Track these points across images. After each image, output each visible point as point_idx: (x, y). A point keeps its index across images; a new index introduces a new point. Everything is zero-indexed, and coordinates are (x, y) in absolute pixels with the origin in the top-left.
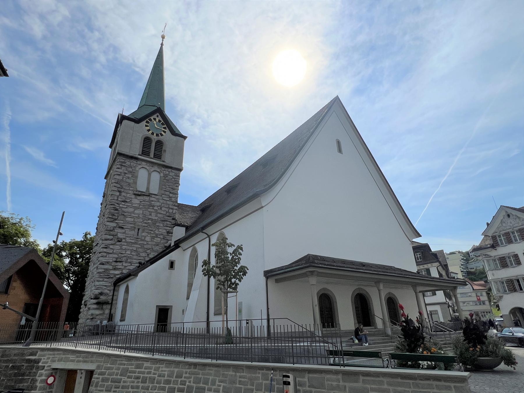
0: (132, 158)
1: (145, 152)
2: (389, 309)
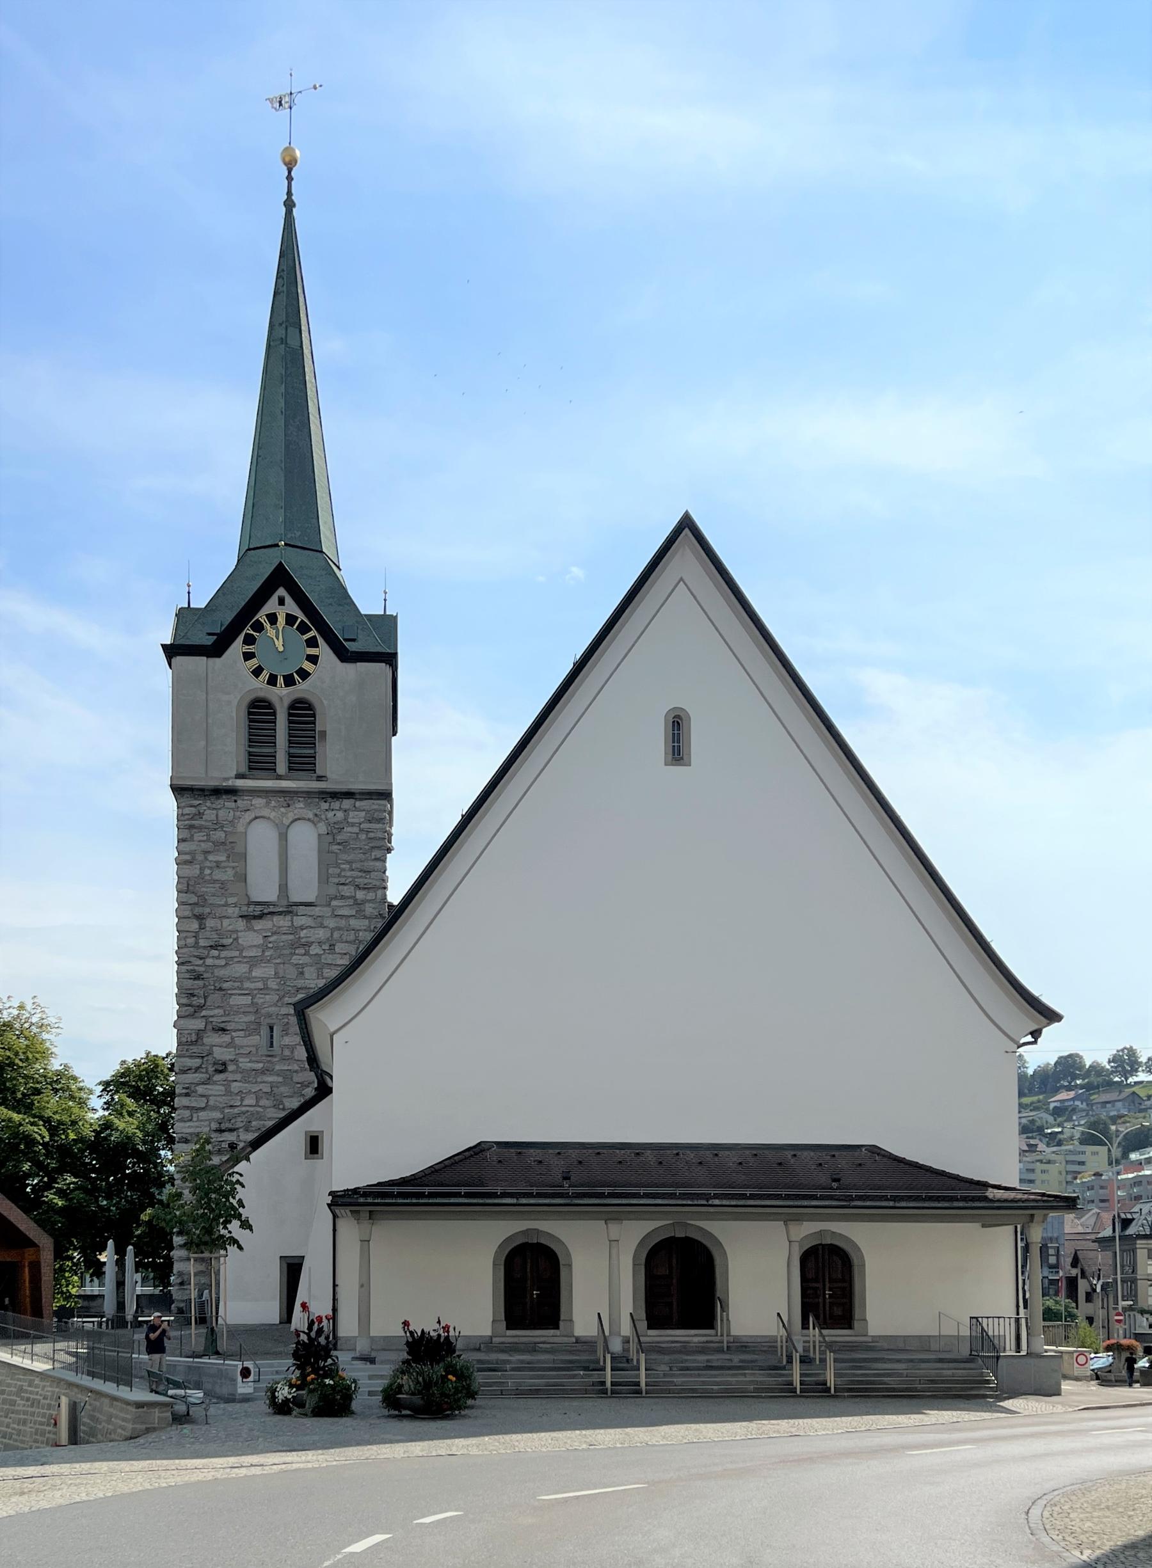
1: (259, 763)
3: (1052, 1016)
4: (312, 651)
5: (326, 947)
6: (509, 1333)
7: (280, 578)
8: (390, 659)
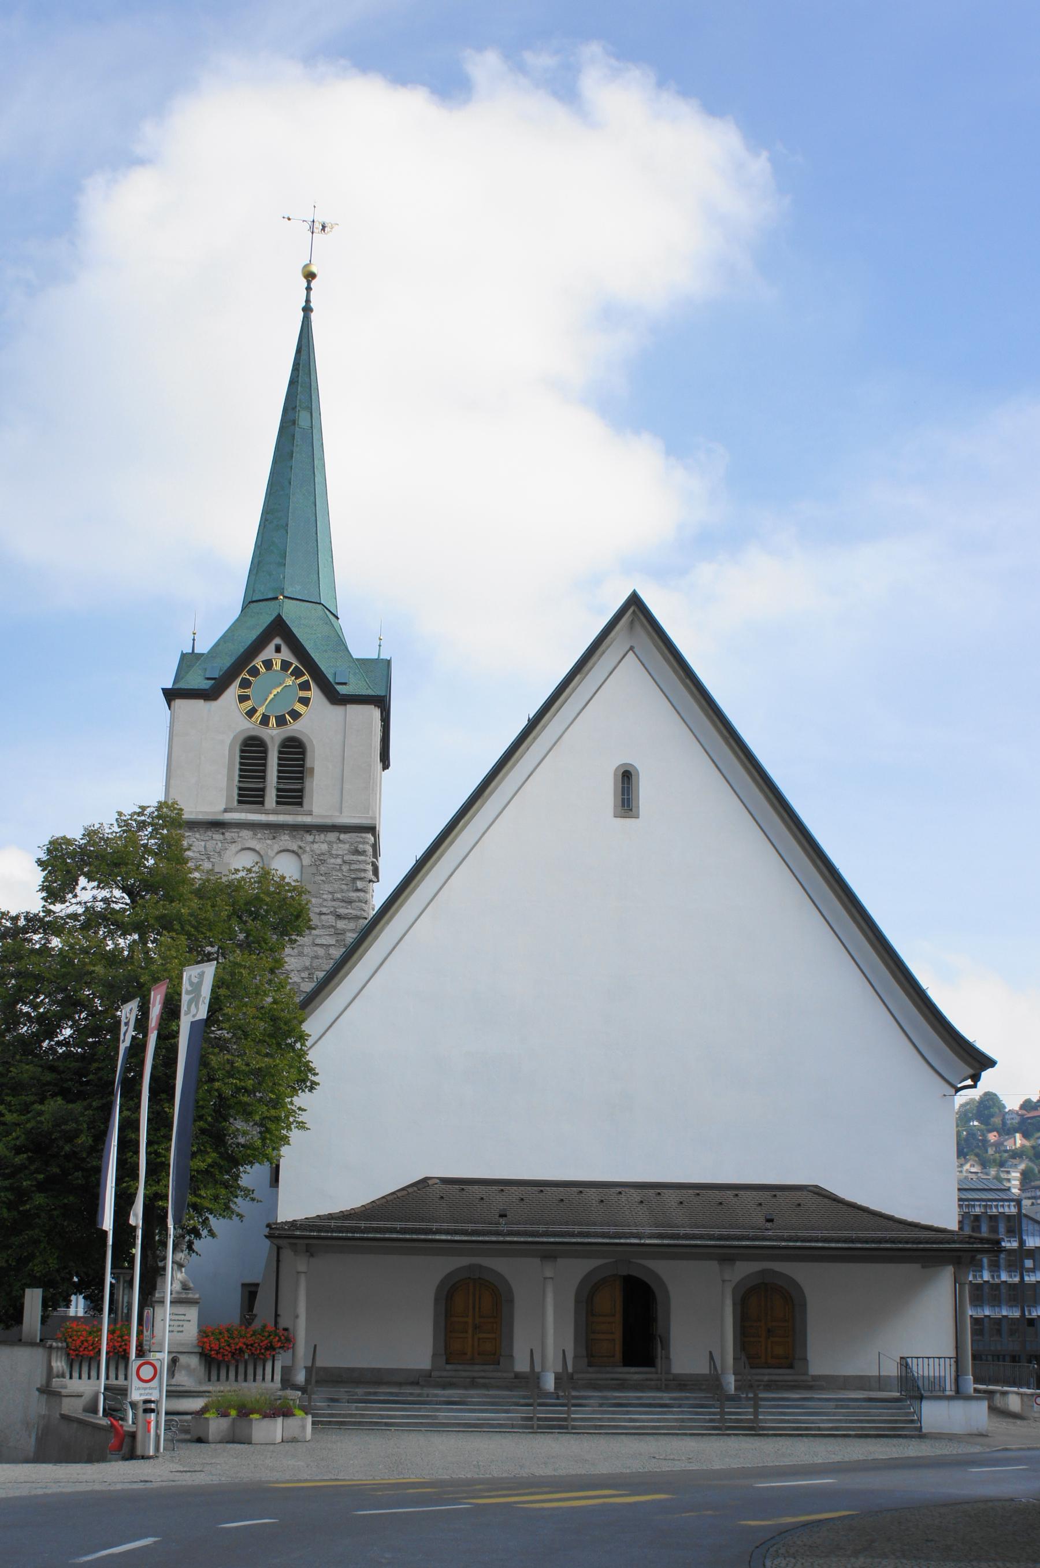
0: (217, 825)
1: (250, 795)
2: (97, 1205)
3: (990, 1063)
4: (302, 694)
5: (305, 975)
6: (448, 1367)
7: (279, 628)
8: (382, 703)
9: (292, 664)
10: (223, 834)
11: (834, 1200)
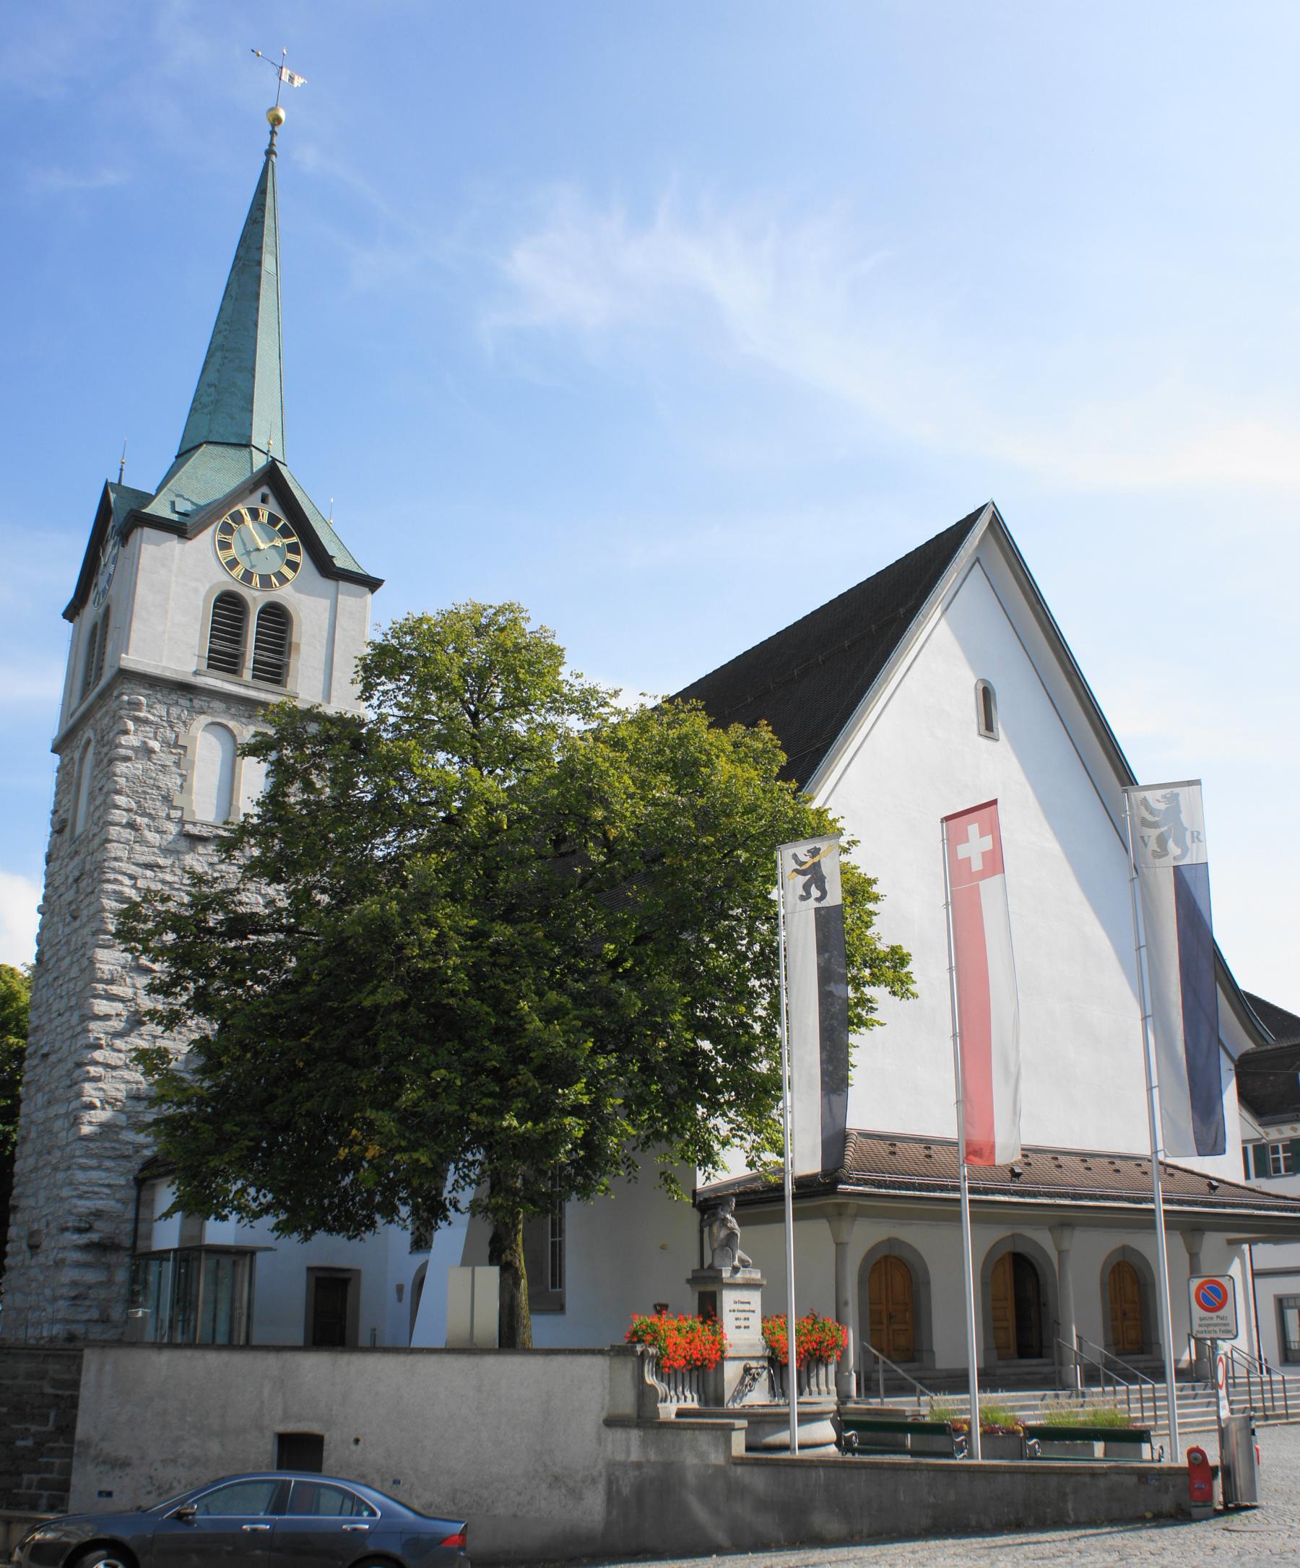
0: (185, 689)
4: (291, 557)
9: (280, 520)
10: (191, 700)
11: (831, 1110)
